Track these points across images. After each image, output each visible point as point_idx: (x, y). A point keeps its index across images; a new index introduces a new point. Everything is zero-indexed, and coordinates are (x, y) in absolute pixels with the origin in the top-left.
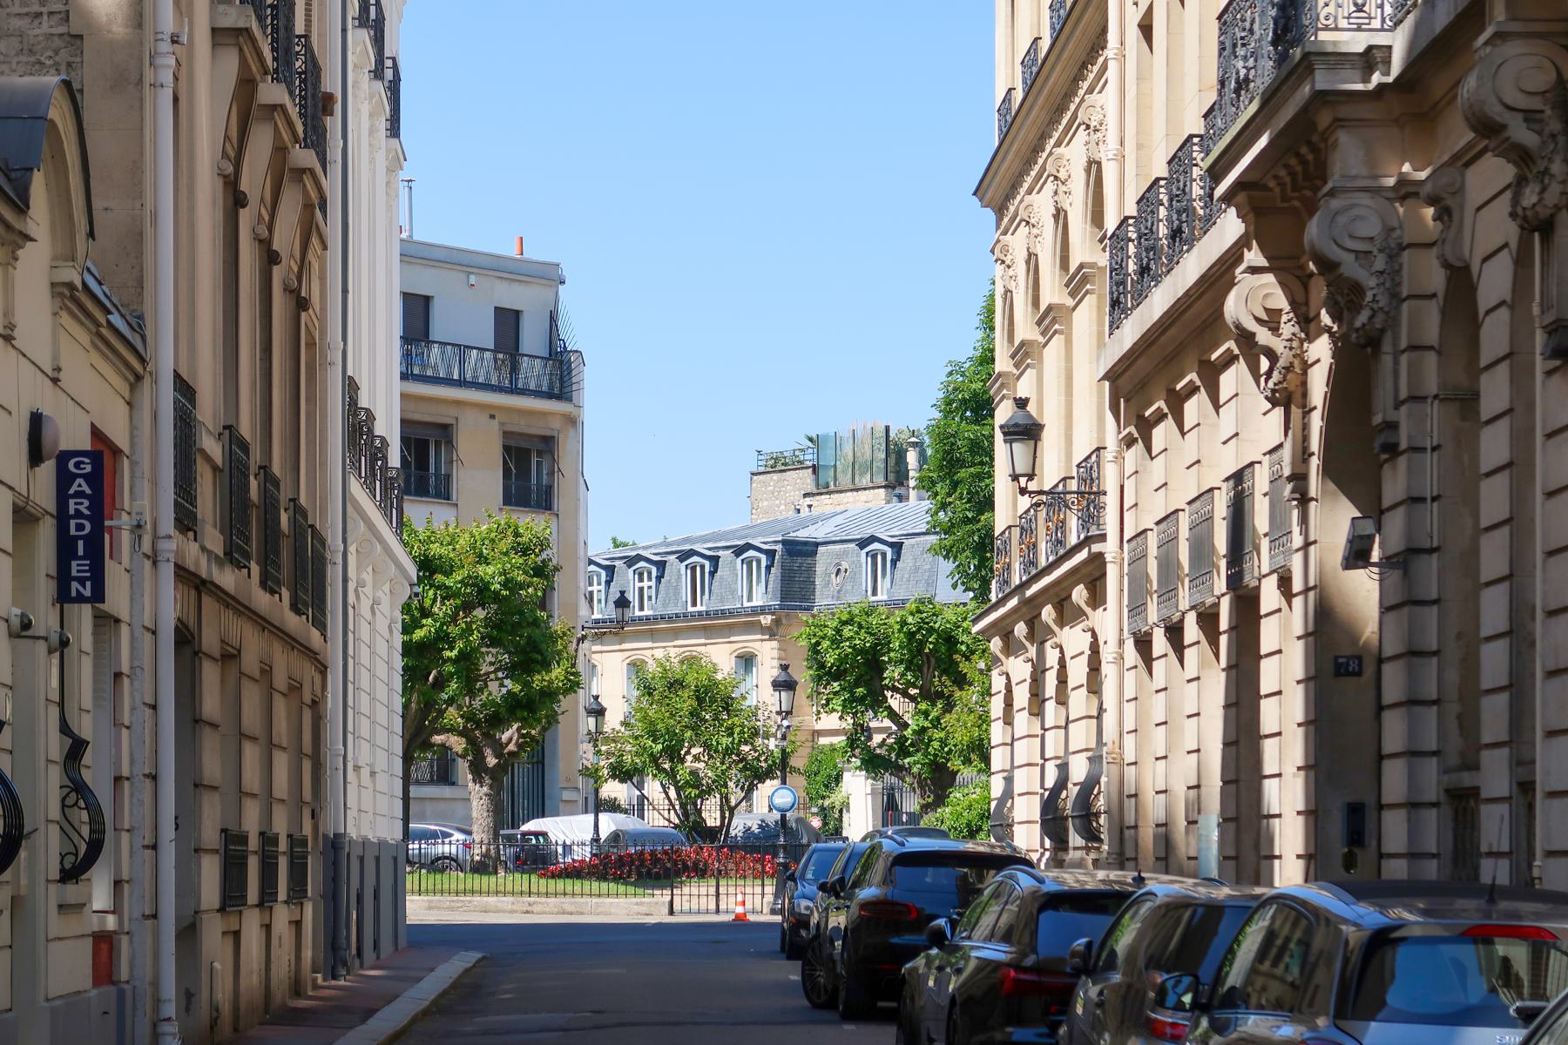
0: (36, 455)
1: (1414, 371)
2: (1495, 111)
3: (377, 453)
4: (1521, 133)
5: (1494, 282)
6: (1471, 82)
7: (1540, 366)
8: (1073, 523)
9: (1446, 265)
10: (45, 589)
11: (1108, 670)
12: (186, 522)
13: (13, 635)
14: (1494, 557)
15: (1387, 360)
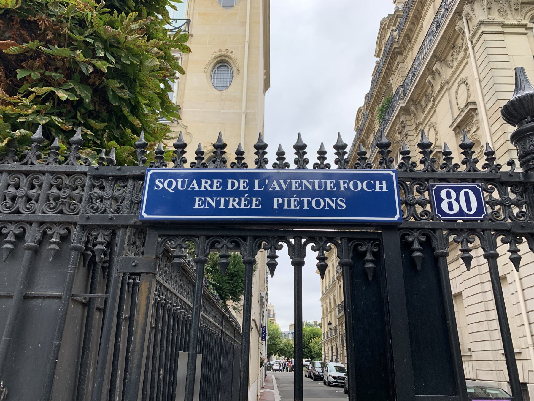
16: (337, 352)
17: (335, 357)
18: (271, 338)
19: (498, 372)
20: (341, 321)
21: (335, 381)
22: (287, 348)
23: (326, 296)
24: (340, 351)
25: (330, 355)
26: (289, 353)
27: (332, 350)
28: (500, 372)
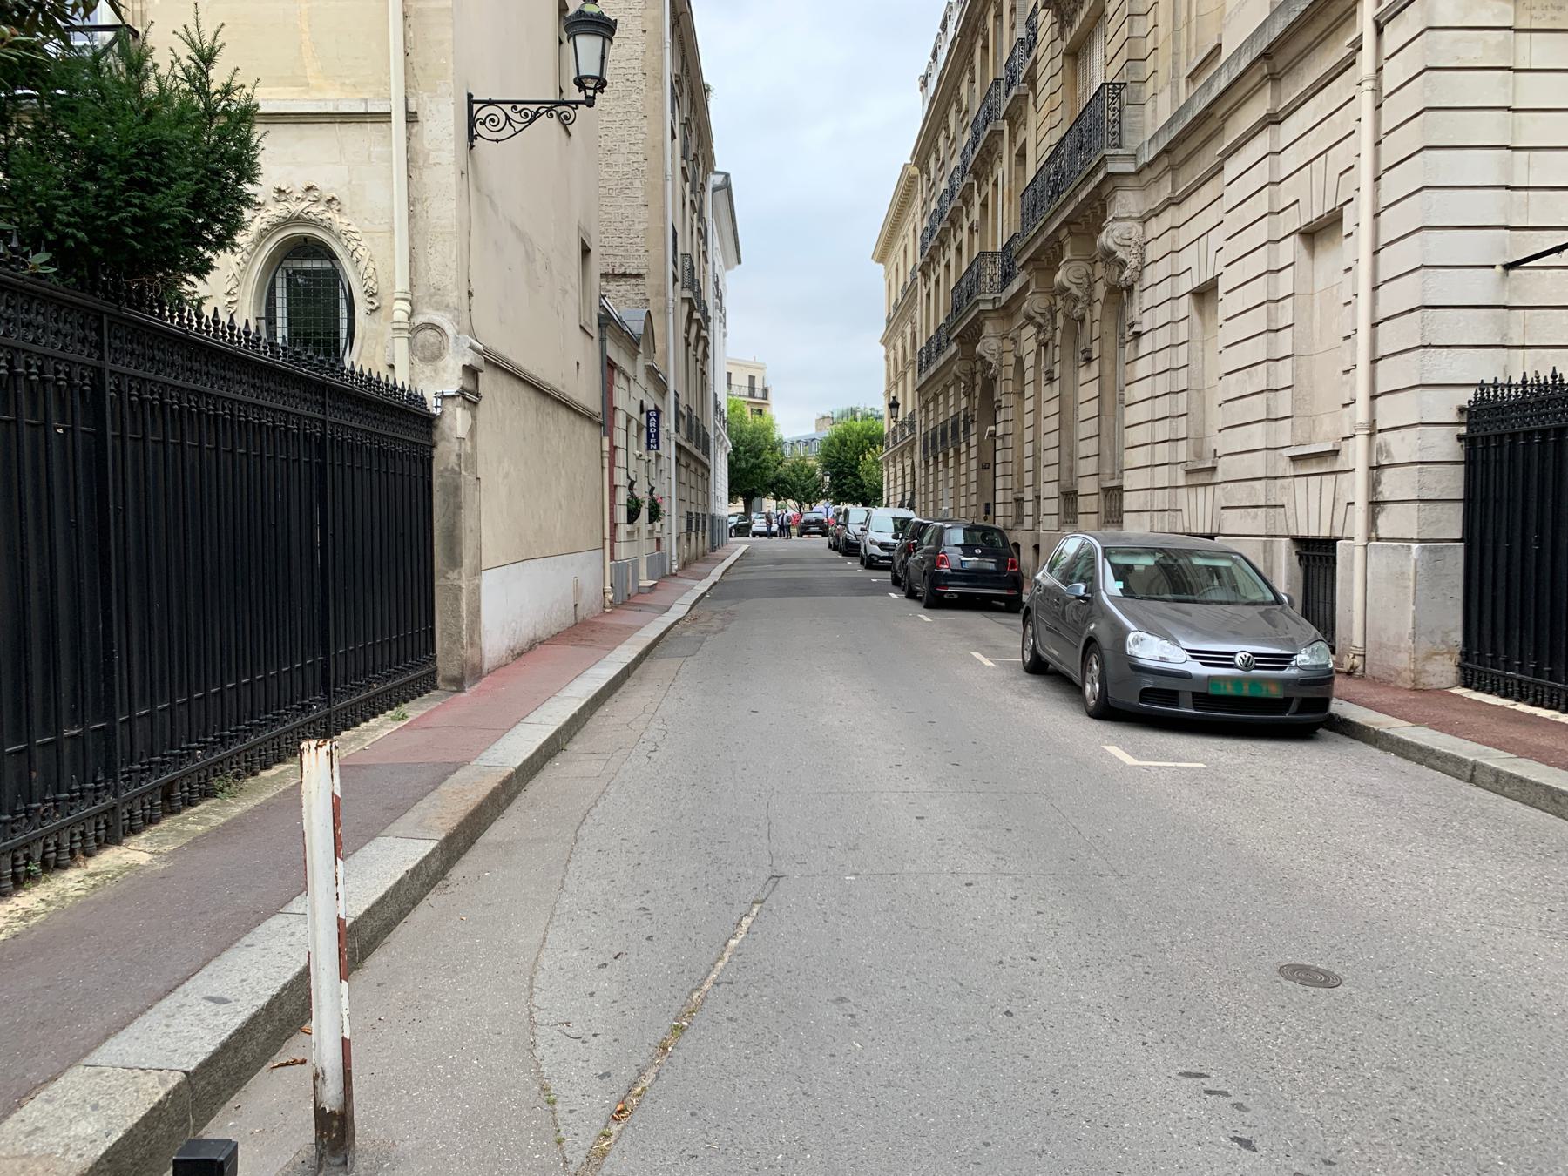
0: (642, 412)
1: (1006, 385)
2: (1032, 314)
3: (722, 413)
4: (1039, 319)
5: (1029, 361)
6: (1025, 305)
7: (1043, 383)
8: (907, 430)
9: (1015, 356)
10: (644, 447)
11: (917, 469)
12: (677, 430)
13: (637, 459)
14: (1028, 435)
15: (998, 383)
16: (913, 481)
17: (908, 496)
18: (750, 451)
19: (1272, 511)
20: (925, 398)
21: (886, 554)
22: (797, 476)
23: (895, 329)
24: (921, 477)
25: (899, 490)
26: (803, 489)
27: (904, 477)
28: (1278, 510)
